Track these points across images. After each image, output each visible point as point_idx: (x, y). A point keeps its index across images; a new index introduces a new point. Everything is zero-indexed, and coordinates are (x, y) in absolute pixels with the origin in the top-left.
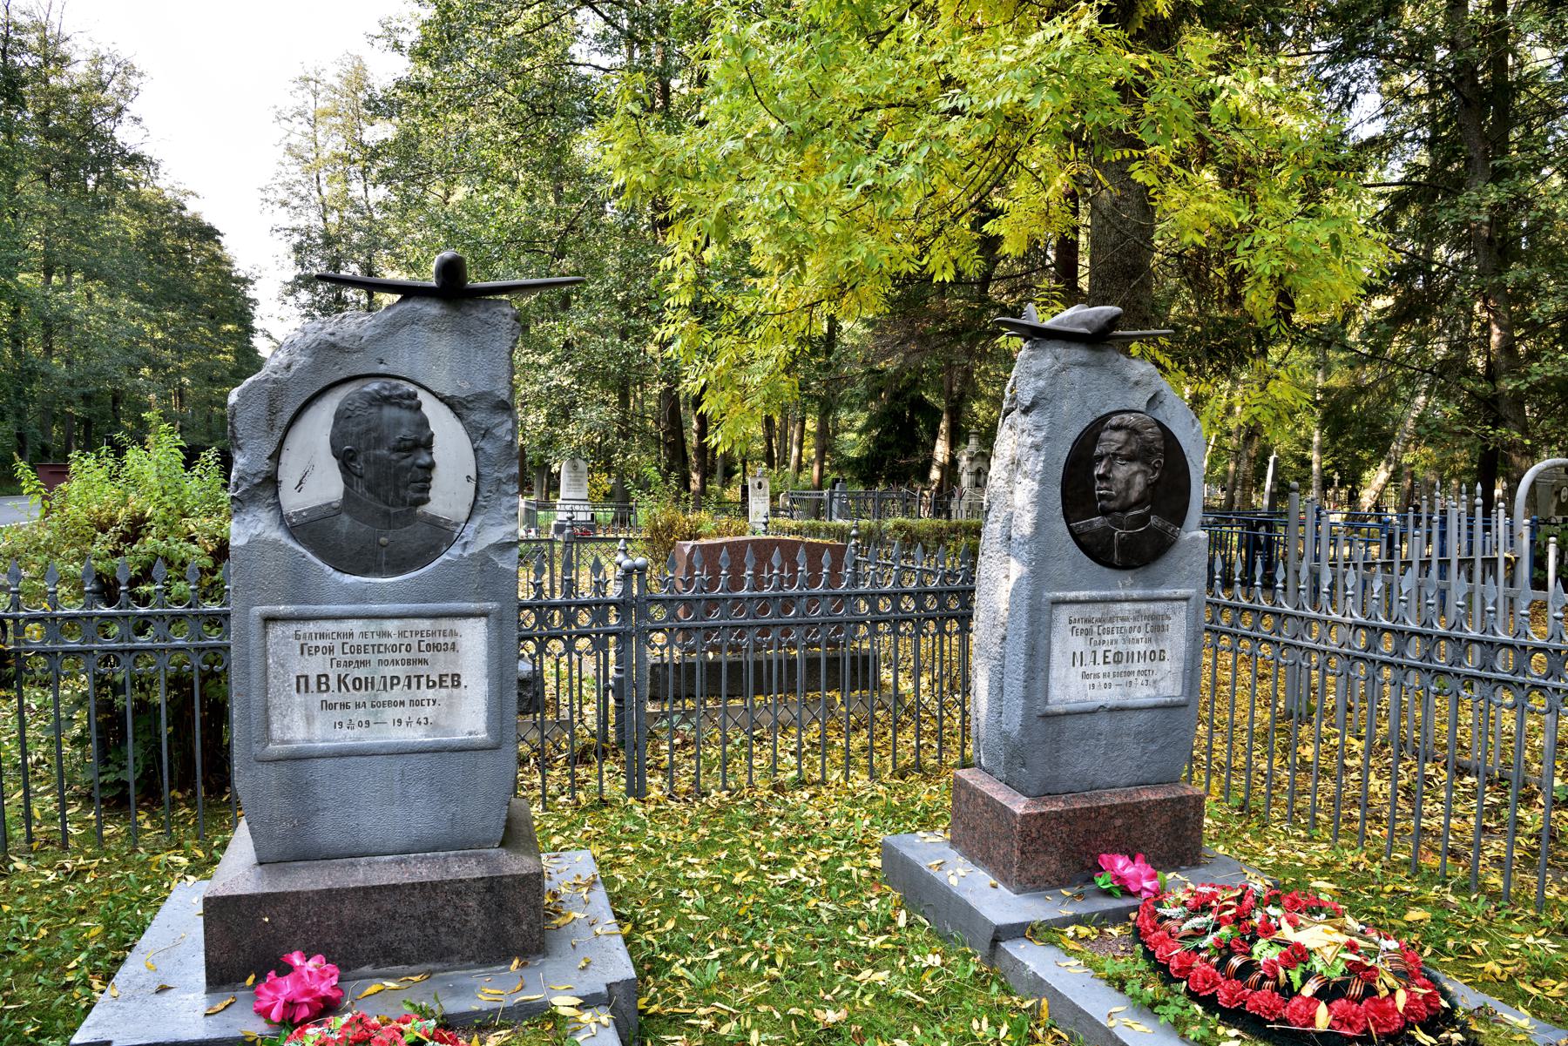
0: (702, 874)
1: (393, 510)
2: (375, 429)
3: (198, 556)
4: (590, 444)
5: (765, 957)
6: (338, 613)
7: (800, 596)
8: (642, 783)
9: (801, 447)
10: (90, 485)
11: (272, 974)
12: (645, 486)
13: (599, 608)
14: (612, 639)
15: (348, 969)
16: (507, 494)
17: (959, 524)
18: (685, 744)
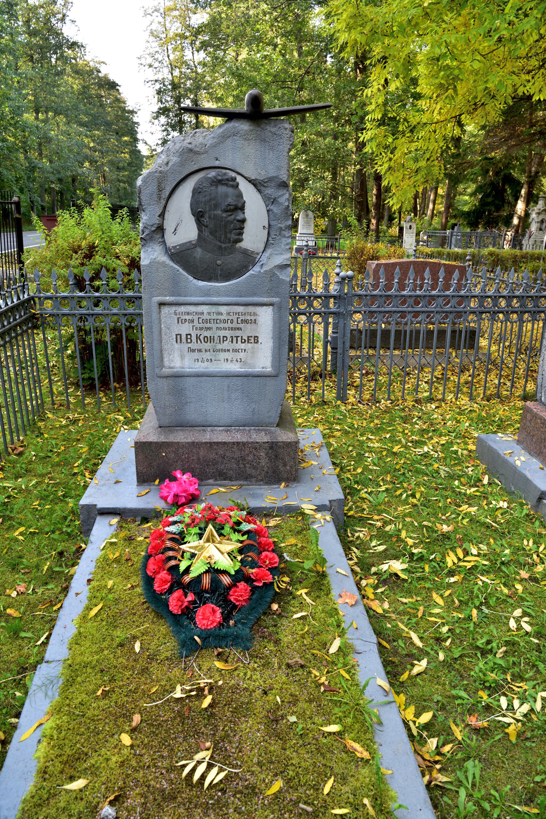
0: (377, 445)
1: (223, 246)
3: (121, 266)
4: (315, 202)
5: (410, 493)
6: (196, 302)
8: (345, 394)
9: (434, 204)
11: (167, 480)
12: (348, 225)
15: (202, 480)
17: (527, 253)
18: (367, 373)
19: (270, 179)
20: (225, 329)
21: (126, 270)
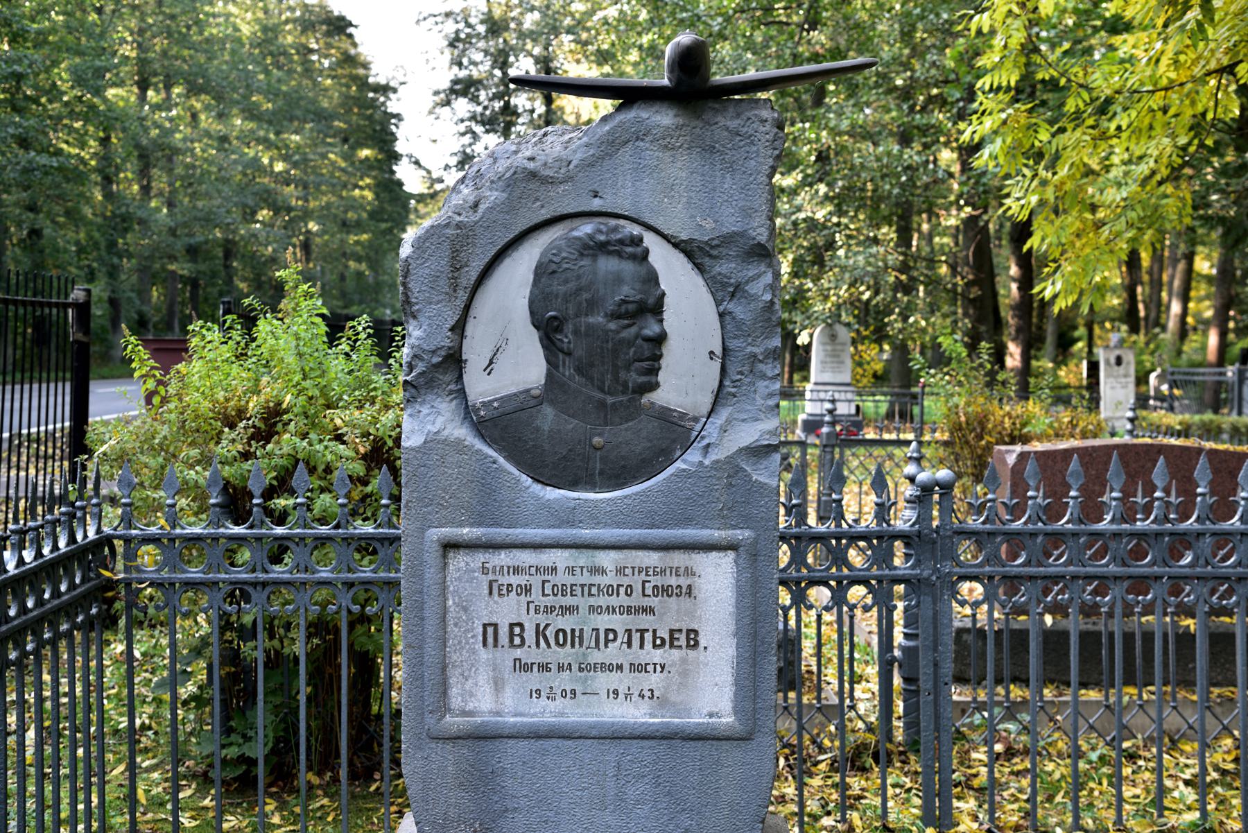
1: (610, 400)
2: (588, 288)
3: (346, 458)
4: (854, 302)
6: (538, 540)
7: (1200, 535)
8: (947, 809)
9: (1185, 299)
10: (212, 367)
12: (939, 359)
13: (881, 540)
14: (900, 589)
16: (763, 376)
18: (1010, 753)
19: (728, 240)
20: (611, 610)
21: (359, 468)
